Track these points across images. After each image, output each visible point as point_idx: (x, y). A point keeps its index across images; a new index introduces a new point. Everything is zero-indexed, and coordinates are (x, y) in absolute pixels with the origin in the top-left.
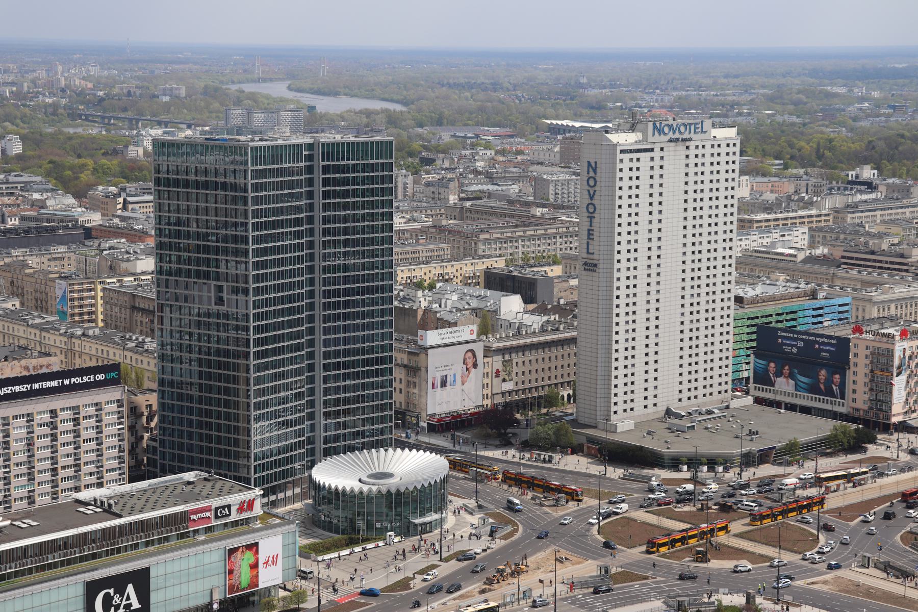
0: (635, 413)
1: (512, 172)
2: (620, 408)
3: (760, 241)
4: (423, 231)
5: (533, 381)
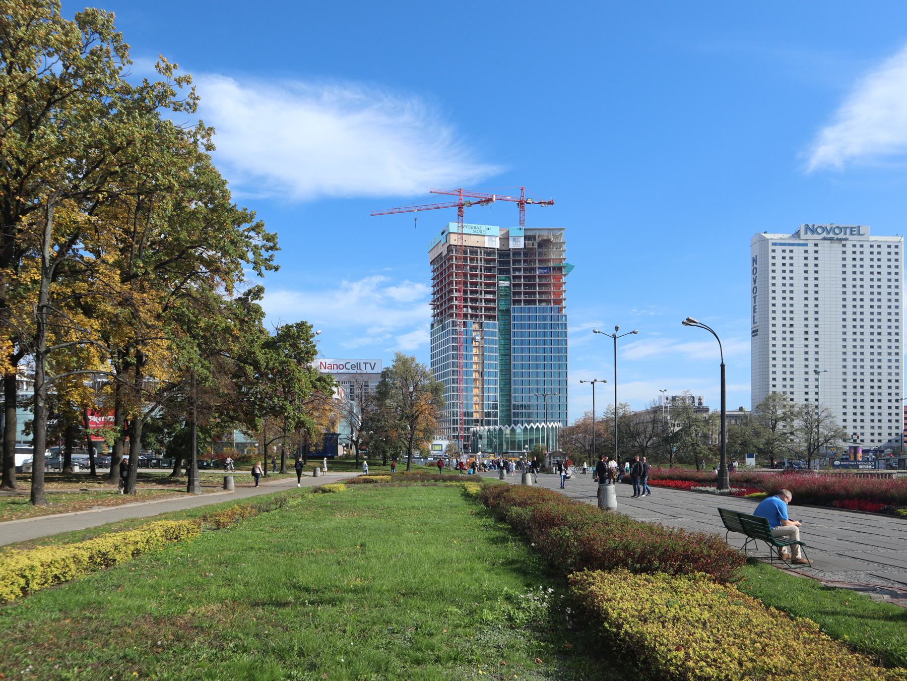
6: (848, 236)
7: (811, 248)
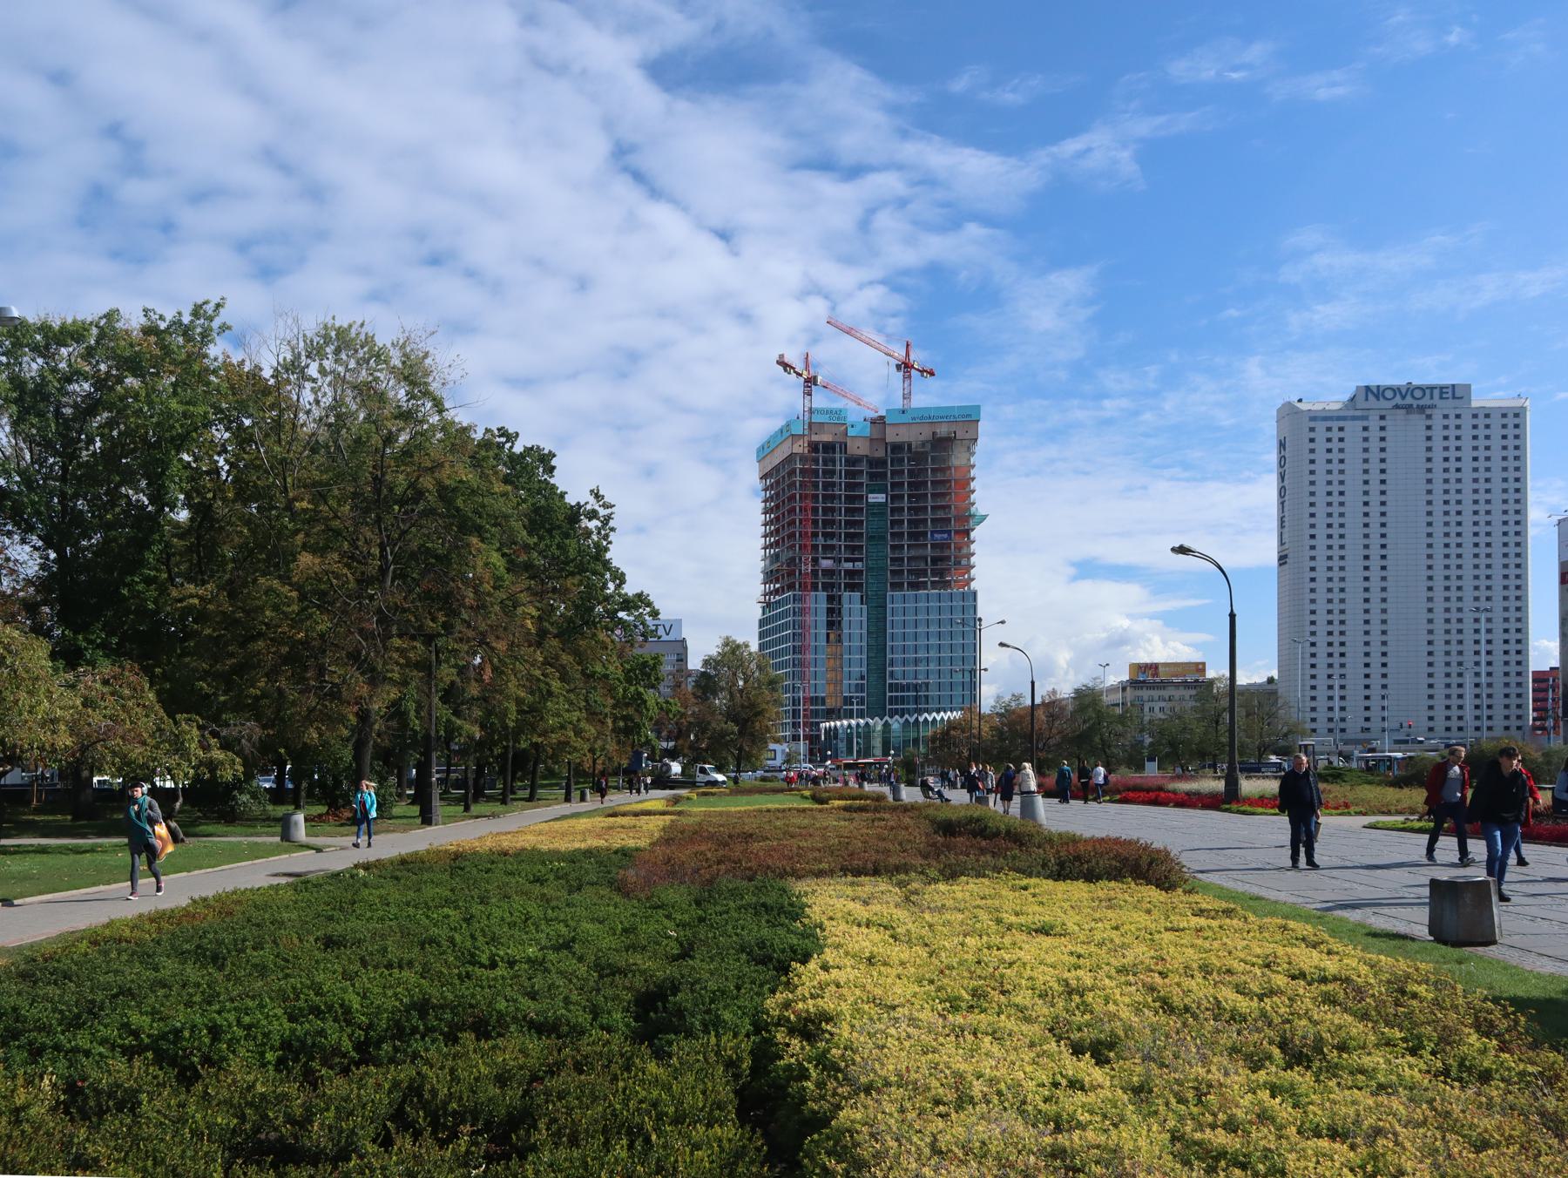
7: (1374, 424)
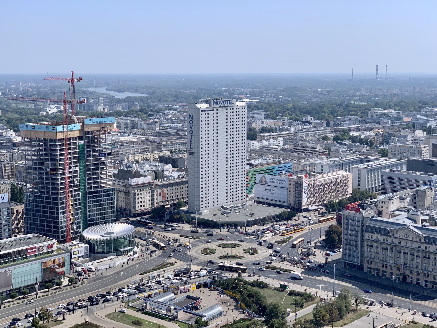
0: (210, 207)
1: (181, 119)
2: (204, 206)
3: (266, 143)
4: (142, 141)
5: (174, 197)
6: (228, 105)
